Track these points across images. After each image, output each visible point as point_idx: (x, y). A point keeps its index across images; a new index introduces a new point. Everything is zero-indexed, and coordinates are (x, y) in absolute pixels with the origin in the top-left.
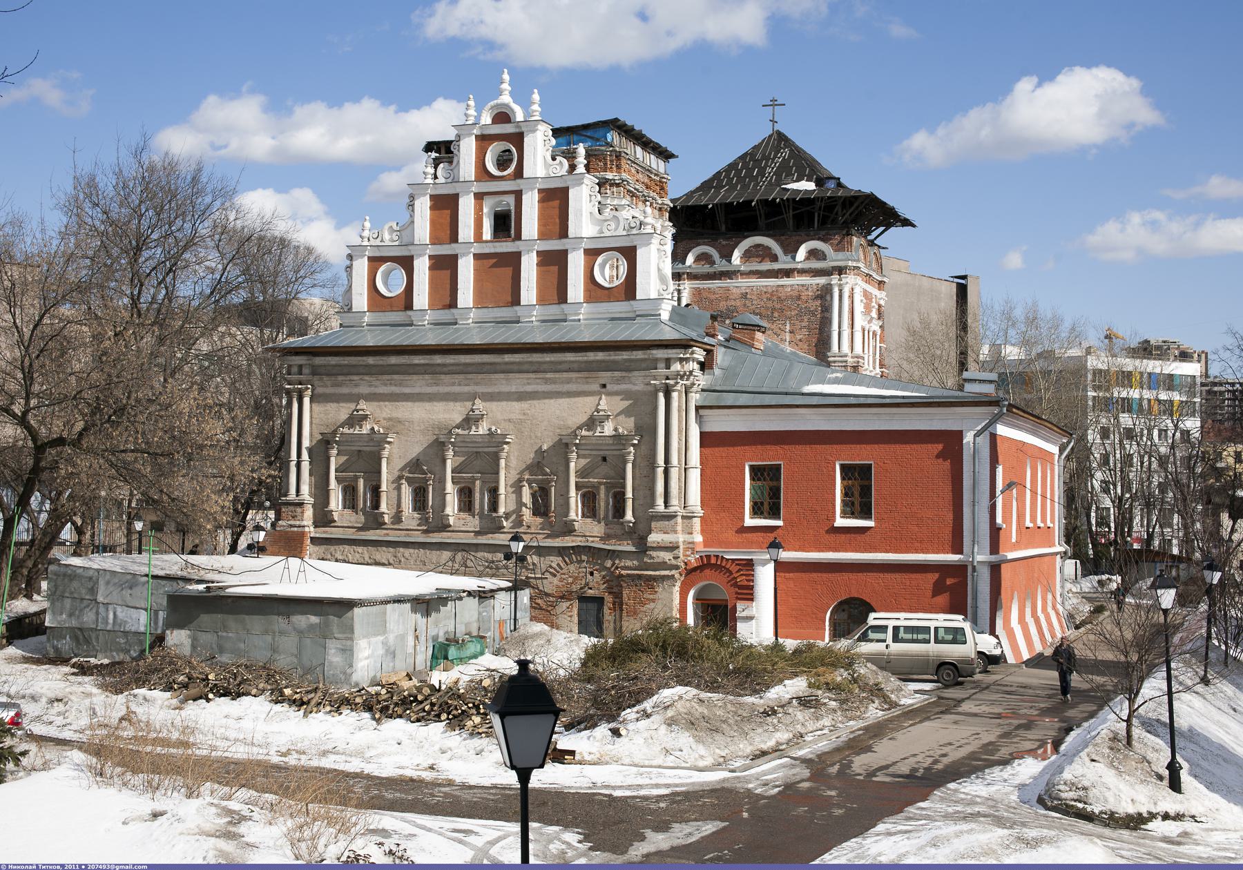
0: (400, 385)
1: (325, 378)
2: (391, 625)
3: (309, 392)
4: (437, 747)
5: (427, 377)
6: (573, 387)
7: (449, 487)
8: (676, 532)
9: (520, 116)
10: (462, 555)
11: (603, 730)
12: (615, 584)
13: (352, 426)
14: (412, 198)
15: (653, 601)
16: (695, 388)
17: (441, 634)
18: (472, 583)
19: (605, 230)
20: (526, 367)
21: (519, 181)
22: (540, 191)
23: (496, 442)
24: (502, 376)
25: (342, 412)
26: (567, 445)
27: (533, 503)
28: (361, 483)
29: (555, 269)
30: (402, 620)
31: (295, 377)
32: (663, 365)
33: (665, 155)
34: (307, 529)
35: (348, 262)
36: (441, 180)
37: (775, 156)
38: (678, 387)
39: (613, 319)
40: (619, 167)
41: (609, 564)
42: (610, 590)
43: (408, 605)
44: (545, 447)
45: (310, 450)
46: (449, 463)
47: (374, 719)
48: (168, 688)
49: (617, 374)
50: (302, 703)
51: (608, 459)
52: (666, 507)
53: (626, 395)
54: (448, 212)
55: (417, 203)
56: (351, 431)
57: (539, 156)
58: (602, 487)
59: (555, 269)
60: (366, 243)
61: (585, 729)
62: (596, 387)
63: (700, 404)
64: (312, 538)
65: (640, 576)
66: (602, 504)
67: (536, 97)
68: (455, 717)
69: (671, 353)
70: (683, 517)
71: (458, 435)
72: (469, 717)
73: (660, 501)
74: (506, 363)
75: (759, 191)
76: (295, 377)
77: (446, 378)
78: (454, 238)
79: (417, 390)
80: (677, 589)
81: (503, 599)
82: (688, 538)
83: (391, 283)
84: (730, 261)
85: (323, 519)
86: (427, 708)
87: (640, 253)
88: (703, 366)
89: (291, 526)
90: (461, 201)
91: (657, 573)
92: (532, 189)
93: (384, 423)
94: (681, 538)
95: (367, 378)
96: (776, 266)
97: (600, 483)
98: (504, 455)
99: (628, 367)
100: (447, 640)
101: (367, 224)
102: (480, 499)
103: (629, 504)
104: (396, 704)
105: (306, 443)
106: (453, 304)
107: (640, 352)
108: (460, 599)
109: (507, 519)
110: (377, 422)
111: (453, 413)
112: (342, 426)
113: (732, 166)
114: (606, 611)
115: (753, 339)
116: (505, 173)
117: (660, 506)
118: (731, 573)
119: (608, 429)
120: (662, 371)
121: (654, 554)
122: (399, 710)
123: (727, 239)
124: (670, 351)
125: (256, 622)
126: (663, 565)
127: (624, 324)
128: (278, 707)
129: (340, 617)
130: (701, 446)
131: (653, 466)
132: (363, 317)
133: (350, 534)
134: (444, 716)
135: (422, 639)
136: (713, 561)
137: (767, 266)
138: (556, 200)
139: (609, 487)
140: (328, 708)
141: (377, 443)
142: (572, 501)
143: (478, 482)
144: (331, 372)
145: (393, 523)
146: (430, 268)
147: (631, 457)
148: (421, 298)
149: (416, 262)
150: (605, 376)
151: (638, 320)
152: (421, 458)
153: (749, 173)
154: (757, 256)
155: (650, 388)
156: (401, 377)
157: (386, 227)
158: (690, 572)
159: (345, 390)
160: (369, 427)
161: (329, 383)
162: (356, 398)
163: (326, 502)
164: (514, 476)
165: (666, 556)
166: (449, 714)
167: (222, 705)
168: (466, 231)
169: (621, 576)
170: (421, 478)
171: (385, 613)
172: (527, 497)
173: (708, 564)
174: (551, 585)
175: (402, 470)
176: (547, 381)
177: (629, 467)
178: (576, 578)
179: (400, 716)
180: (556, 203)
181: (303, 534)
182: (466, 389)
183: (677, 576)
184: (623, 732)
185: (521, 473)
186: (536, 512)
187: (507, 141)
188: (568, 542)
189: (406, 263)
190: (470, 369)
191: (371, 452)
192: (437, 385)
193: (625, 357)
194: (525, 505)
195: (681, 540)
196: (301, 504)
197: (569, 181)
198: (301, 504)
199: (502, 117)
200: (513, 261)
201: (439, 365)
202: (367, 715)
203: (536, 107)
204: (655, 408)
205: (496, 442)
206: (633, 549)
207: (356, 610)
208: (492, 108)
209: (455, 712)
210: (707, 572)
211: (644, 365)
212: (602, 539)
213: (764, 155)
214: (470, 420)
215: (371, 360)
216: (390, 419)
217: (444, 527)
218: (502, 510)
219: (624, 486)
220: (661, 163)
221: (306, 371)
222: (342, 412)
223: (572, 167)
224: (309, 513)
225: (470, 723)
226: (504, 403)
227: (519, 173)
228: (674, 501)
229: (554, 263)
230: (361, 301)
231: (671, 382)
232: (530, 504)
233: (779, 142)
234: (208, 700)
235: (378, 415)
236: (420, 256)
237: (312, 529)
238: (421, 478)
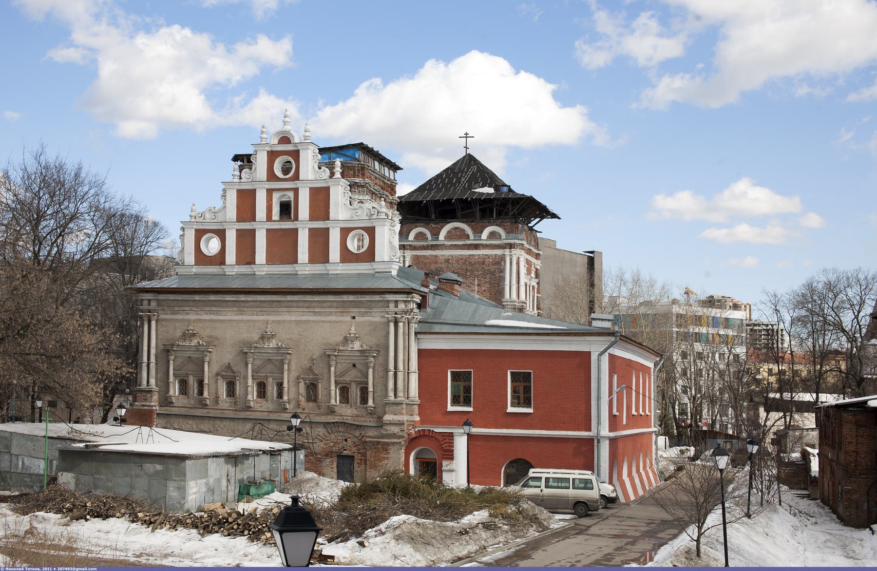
8: (402, 414)
11: (353, 542)
15: (387, 458)
16: (414, 320)
18: (266, 445)
24: (286, 309)
33: (395, 168)
35: (182, 233)
41: (357, 434)
63: (418, 330)
65: (378, 443)
68: (254, 533)
72: (263, 533)
73: (391, 394)
74: (289, 301)
75: (457, 194)
81: (287, 457)
83: (212, 246)
85: (166, 401)
88: (419, 306)
89: (143, 406)
96: (468, 242)
99: (370, 305)
104: (214, 524)
105: (153, 351)
108: (258, 455)
110: (202, 338)
115: (453, 289)
116: (287, 177)
119: (357, 346)
122: (216, 528)
123: (436, 224)
126: (394, 436)
131: (387, 371)
133: (183, 411)
134: (246, 532)
135: (232, 481)
148: (231, 257)
158: (412, 441)
160: (196, 341)
168: (261, 212)
171: (207, 464)
179: (217, 532)
184: (366, 544)
189: (221, 234)
197: (330, 183)
198: (150, 392)
204: (388, 333)
207: (188, 462)
210: (423, 440)
213: (460, 169)
219: (367, 383)
224: (156, 397)
225: (263, 537)
227: (296, 177)
228: (400, 394)
229: (320, 239)
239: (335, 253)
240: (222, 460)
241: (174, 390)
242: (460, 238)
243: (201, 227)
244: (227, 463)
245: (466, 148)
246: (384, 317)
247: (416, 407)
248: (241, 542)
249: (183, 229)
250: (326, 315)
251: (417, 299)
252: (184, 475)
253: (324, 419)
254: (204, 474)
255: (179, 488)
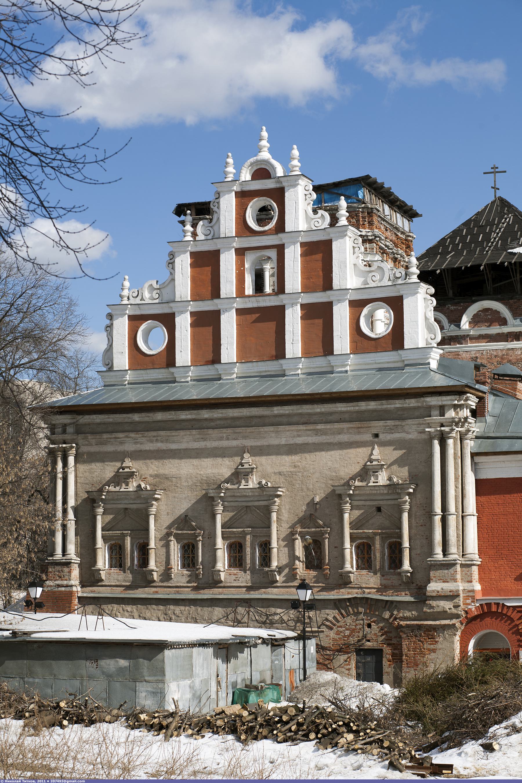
0: (167, 441)
1: (90, 437)
2: (197, 669)
3: (74, 451)
4: (312, 765)
5: (194, 432)
6: (344, 438)
7: (220, 543)
8: (455, 580)
9: (280, 172)
10: (233, 609)
11: (472, 747)
12: (394, 635)
13: (118, 484)
14: (172, 256)
15: (434, 651)
16: (470, 435)
17: (239, 681)
18: (264, 633)
19: (369, 281)
20: (295, 419)
21: (281, 235)
22: (302, 245)
23: (267, 495)
24: (271, 428)
25: (109, 470)
26: (340, 496)
27: (306, 556)
28: (128, 541)
29: (319, 322)
30: (205, 662)
31: (61, 437)
32: (437, 412)
33: (410, 213)
34: (74, 589)
35: (108, 322)
36: (201, 237)
37: (499, 222)
38: (453, 434)
39: (380, 370)
40: (371, 224)
41: (387, 615)
42: (388, 642)
43: (210, 650)
44: (317, 499)
45: (76, 510)
46: (219, 518)
47: (239, 739)
48: (19, 715)
49: (390, 423)
50: (160, 728)
51: (382, 509)
52: (445, 555)
53: (397, 444)
54: (209, 269)
55: (178, 261)
56: (117, 489)
57: (301, 212)
58: (378, 538)
59: (319, 322)
60: (125, 302)
61: (450, 748)
62: (368, 437)
63: (475, 450)
64: (79, 598)
65: (419, 627)
66: (378, 555)
67: (296, 152)
68: (324, 735)
69: (445, 400)
70: (462, 565)
71: (227, 489)
72: (340, 735)
73: (438, 550)
74: (276, 416)
75: (486, 256)
76: (61, 437)
77: (214, 433)
78: (216, 293)
79: (183, 446)
80: (457, 638)
81: (293, 648)
82: (467, 586)
83: (153, 342)
84: (459, 326)
85: (90, 578)
86: (293, 728)
87: (406, 302)
88: (474, 413)
89: (59, 586)
90: (222, 257)
91: (438, 623)
92: (294, 243)
93: (150, 479)
94: (461, 586)
95: (132, 435)
96: (505, 330)
97: (375, 534)
98: (275, 508)
99: (401, 416)
100: (246, 686)
101: (127, 284)
102: (251, 554)
103: (406, 554)
104: (261, 725)
105: (71, 502)
106: (216, 359)
107: (413, 400)
108: (255, 646)
109: (280, 573)
110: (144, 480)
111: (222, 468)
112: (108, 484)
113: (456, 233)
114: (385, 663)
115: (515, 389)
116: (266, 228)
117: (439, 555)
118: (512, 620)
119: (382, 479)
120: (436, 418)
121: (434, 603)
122: (265, 732)
123: (455, 304)
124: (444, 398)
125: (63, 668)
126: (444, 615)
127: (393, 374)
128: (136, 733)
129: (150, 660)
130: (477, 494)
131: (430, 514)
132: (124, 376)
133: (118, 593)
134: (312, 736)
135: (223, 685)
136: (494, 609)
137: (495, 330)
138: (319, 253)
139: (384, 537)
140: (190, 732)
141: (144, 500)
142: (347, 552)
143: (248, 537)
144: (95, 431)
145: (162, 581)
146: (192, 325)
147: (407, 507)
148: (184, 355)
149: (177, 320)
150: (377, 426)
151: (407, 369)
152: (190, 514)
153: (475, 237)
154: (486, 321)
155: (424, 436)
156: (168, 433)
157: (147, 285)
158: (472, 620)
159: (109, 448)
160: (135, 484)
161: (93, 441)
162: (120, 456)
163: (94, 561)
164: (285, 530)
165: (447, 605)
166: (317, 734)
167: (74, 733)
168: (228, 286)
169: (400, 627)
170: (190, 533)
171: (191, 657)
172: (299, 552)
173: (488, 612)
174: (329, 637)
175: (169, 527)
176: (317, 432)
177: (405, 516)
178: (353, 631)
179: (266, 738)
180: (319, 256)
181: (71, 593)
182: (234, 443)
183: (458, 625)
184: (496, 747)
185: (293, 527)
186: (309, 566)
187: (268, 198)
188: (344, 594)
189: (168, 321)
190: (238, 423)
191: (138, 510)
192: (204, 439)
193: (393, 405)
194: (298, 559)
195: (461, 588)
196: (68, 564)
197: (332, 233)
198: (68, 564)
199: (262, 173)
200: (277, 315)
201: (206, 419)
202: (230, 737)
203: (296, 162)
204: (431, 456)
205: (267, 495)
206: (412, 599)
207: (168, 653)
208: (252, 164)
209: (325, 731)
210: (488, 620)
211: (417, 413)
212: (379, 590)
213: (487, 221)
214: (238, 475)
215: (136, 417)
216: (156, 476)
217: (216, 583)
218: (274, 564)
219: (400, 536)
220: (406, 222)
221: (70, 430)
222: (109, 470)
223: (334, 220)
224: (76, 572)
225: (342, 741)
226: (274, 457)
227: (280, 227)
228: (453, 549)
229: (319, 316)
230: (122, 360)
231: (447, 429)
232: (302, 557)
233: (502, 208)
234: (62, 727)
235: (144, 473)
236: (182, 312)
237: (79, 589)
238: (190, 533)
239: (342, 340)
240: (210, 651)
241: (103, 560)
242: (490, 323)
243: (138, 313)
244: (216, 655)
245: (495, 188)
246: (424, 432)
247: (475, 569)
248: (306, 749)
249: (110, 317)
250: (333, 434)
251: (473, 402)
252: (162, 672)
253: (333, 595)
254: (188, 671)
255: (154, 693)
